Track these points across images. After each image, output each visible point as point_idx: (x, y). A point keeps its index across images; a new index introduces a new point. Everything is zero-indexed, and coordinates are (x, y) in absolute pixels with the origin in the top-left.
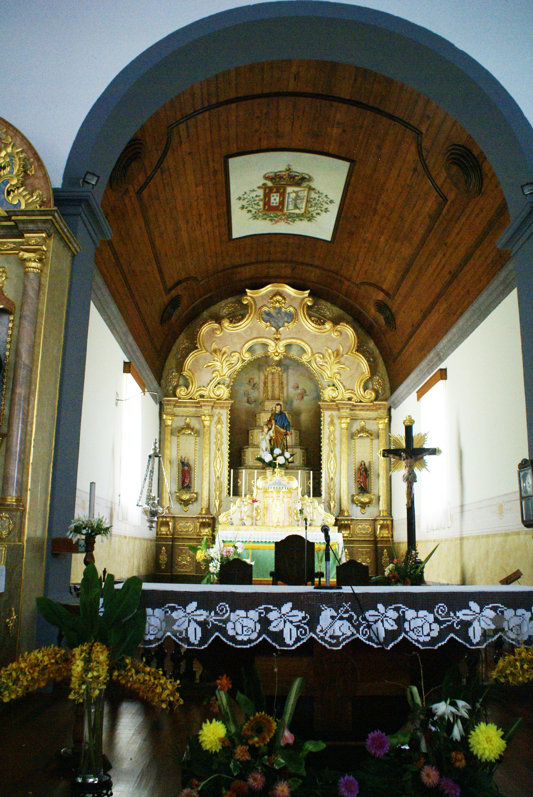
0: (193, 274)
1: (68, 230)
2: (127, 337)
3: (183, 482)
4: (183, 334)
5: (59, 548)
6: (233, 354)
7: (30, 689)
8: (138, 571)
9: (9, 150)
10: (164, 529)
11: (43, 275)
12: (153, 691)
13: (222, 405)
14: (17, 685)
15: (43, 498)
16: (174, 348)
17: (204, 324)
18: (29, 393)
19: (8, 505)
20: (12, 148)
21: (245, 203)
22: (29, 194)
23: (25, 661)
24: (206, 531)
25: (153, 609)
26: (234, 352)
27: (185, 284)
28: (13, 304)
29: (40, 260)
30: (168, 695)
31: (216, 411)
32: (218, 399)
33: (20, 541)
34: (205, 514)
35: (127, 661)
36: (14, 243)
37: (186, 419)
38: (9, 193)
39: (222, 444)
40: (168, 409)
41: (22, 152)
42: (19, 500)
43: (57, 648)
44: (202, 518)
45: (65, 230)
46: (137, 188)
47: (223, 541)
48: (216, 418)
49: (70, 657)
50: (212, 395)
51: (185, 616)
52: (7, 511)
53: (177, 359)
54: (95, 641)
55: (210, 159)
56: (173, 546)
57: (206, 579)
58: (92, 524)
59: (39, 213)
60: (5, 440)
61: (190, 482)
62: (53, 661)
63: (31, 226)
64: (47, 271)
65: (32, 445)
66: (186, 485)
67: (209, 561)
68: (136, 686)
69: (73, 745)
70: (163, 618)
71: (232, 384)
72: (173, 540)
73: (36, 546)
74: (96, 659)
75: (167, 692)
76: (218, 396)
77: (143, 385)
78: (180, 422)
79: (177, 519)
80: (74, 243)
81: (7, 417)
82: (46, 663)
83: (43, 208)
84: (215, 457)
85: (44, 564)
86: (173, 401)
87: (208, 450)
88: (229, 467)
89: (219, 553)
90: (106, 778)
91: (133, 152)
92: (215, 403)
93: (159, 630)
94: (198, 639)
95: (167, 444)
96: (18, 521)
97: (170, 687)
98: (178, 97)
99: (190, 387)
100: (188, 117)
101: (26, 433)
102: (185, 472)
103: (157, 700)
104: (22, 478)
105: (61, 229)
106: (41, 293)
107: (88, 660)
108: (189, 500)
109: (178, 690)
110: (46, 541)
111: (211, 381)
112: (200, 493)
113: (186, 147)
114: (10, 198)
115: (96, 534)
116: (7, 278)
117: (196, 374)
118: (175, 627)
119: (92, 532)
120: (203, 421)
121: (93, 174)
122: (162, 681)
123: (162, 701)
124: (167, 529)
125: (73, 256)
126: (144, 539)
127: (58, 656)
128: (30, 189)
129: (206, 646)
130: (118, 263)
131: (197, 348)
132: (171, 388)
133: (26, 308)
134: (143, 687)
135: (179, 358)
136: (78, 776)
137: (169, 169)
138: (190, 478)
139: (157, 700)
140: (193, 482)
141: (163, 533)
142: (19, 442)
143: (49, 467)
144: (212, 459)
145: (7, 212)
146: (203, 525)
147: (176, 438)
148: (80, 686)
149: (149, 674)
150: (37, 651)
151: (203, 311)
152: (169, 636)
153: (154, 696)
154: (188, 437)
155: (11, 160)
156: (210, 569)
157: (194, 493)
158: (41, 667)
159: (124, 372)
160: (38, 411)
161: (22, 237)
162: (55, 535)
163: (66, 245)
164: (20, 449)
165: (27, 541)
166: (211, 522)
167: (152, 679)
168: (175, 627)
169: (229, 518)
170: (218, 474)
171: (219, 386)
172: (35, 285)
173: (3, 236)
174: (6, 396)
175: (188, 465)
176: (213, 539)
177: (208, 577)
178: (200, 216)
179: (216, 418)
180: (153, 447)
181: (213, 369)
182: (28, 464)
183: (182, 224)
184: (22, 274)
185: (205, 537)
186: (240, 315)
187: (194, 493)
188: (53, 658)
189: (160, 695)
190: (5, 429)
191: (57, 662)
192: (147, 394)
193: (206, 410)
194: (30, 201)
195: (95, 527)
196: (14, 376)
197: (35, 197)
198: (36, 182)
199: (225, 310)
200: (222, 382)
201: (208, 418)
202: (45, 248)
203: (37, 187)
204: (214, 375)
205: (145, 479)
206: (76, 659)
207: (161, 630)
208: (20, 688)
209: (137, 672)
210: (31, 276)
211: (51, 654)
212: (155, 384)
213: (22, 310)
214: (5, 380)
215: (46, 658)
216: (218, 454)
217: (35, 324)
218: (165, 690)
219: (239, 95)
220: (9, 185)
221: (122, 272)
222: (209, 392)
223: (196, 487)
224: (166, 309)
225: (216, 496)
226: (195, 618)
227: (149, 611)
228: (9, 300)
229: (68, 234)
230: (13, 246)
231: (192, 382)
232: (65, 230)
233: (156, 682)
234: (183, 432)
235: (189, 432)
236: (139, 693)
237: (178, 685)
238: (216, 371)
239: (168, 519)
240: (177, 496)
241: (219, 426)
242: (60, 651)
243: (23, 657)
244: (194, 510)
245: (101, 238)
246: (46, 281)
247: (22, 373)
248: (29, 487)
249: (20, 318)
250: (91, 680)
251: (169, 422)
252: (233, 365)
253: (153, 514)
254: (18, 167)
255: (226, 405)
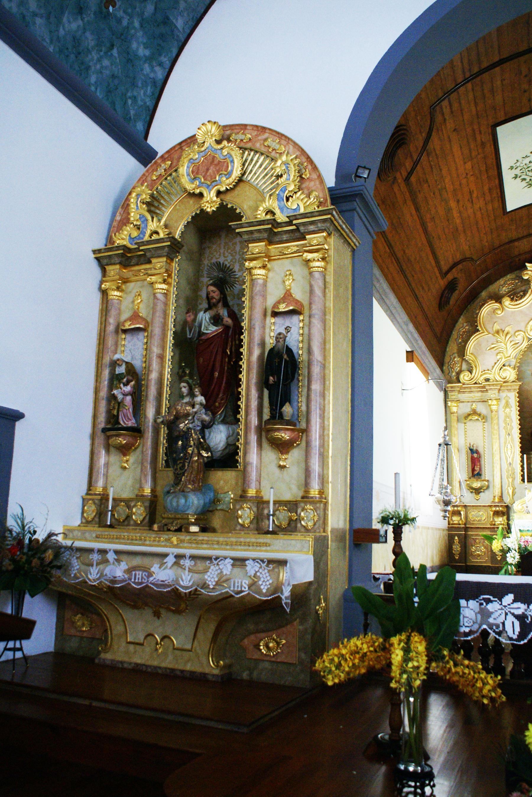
0: (468, 256)
1: (346, 226)
2: (407, 325)
3: (473, 470)
4: (462, 317)
5: (362, 537)
6: (517, 334)
7: (352, 675)
8: (433, 561)
9: (284, 158)
10: (456, 519)
11: (328, 273)
12: (473, 685)
13: (509, 388)
14: (339, 669)
15: (343, 490)
16: (455, 333)
17: (483, 305)
18: (324, 390)
19: (312, 498)
20: (287, 155)
21: (518, 172)
22: (306, 197)
23: (345, 647)
24: (500, 520)
25: (467, 600)
26: (518, 331)
27: (460, 266)
28: (302, 305)
29: (323, 259)
30: (489, 691)
31: (503, 394)
32: (505, 382)
33: (324, 532)
34: (499, 502)
35: (445, 653)
36: (297, 246)
37: (472, 405)
38: (288, 199)
39: (512, 428)
40: (452, 395)
41: (296, 158)
42: (321, 492)
43: (374, 637)
44: (495, 506)
45: (344, 226)
46: (405, 174)
47: (520, 530)
48: (503, 402)
49: (387, 646)
50: (498, 378)
51: (502, 609)
52: (311, 503)
53: (458, 345)
54: (412, 631)
55: (477, 133)
56: (466, 536)
57: (503, 571)
58: (399, 514)
59: (247, 225)
60: (305, 434)
61: (480, 469)
62: (372, 649)
63: (312, 228)
64: (331, 268)
65: (331, 439)
66: (476, 473)
67: (505, 551)
68: (456, 678)
69: (390, 732)
70: (477, 610)
71: (518, 365)
72: (466, 529)
73: (340, 536)
74: (415, 649)
75: (488, 687)
76: (504, 379)
77: (426, 372)
78: (466, 409)
79: (469, 508)
80: (353, 238)
81: (305, 413)
82: (365, 651)
83: (321, 209)
84: (505, 443)
85: (347, 553)
86: (458, 387)
87: (497, 436)
88: (521, 452)
89: (516, 543)
90: (427, 769)
91: (399, 138)
92: (501, 386)
93: (474, 623)
94: (517, 633)
95: (454, 431)
96: (322, 513)
97: (491, 682)
98: (438, 74)
99: (474, 371)
100: (449, 93)
101: (323, 428)
102: (475, 459)
103: (477, 694)
104: (323, 471)
105: (341, 226)
106: (327, 290)
107: (407, 650)
108: (480, 488)
109: (500, 686)
110: (348, 532)
111: (495, 363)
112: (491, 480)
113: (450, 125)
114: (289, 203)
115: (404, 524)
116: (293, 280)
117: (479, 358)
118: (491, 620)
119: (399, 522)
120: (490, 405)
121: (365, 168)
122: (483, 676)
123: (483, 696)
124: (459, 518)
125: (353, 251)
126: (436, 529)
127: (376, 644)
128: (306, 191)
129: (526, 641)
130: (393, 254)
131: (478, 330)
132: (454, 374)
133: (314, 307)
134: (462, 680)
135: (460, 343)
136: (399, 763)
137: (434, 149)
138: (480, 465)
139: (477, 694)
140: (483, 469)
141: (455, 522)
142: (318, 437)
143: (346, 459)
144: (502, 445)
145: (287, 217)
146: (497, 513)
147: (463, 425)
148: (401, 674)
149: (468, 667)
150: (355, 639)
151: (482, 292)
152: (485, 629)
153: (474, 691)
154: (475, 423)
155: (287, 167)
156: (508, 559)
157: (485, 480)
158: (361, 655)
159: (407, 361)
160: (333, 405)
161: (304, 239)
162: (356, 526)
163: (346, 241)
164: (319, 444)
165: (331, 532)
166: (505, 510)
167: (472, 673)
168: (491, 620)
169: (525, 505)
170: (510, 460)
171: (504, 368)
172: (321, 283)
173: (286, 240)
174: (303, 393)
175: (477, 452)
176: (508, 529)
177: (505, 568)
178: (471, 193)
179: (503, 402)
180: (443, 435)
181: (497, 351)
182: (328, 457)
183: (453, 204)
184: (308, 274)
185: (500, 527)
186: (522, 291)
187: (485, 480)
188: (372, 646)
189: (481, 690)
190: (303, 425)
191: (375, 651)
192: (431, 381)
193: (492, 394)
194: (308, 203)
195: (403, 517)
196: (309, 373)
197: (312, 199)
198: (312, 184)
199: (504, 289)
200: (507, 364)
201: (495, 402)
202: (326, 247)
203: (313, 188)
204: (498, 357)
205: (436, 468)
206: (395, 649)
207: (476, 622)
208: (342, 673)
209: (456, 665)
210: (317, 275)
211: (369, 642)
212: (438, 370)
213: (310, 308)
214: (300, 378)
215: (365, 646)
216: (509, 439)
217: (324, 322)
218: (486, 684)
219: (502, 58)
220: (287, 192)
221: (397, 260)
222: (495, 375)
223: (487, 474)
224: (442, 294)
225: (509, 484)
226: (512, 611)
227: (463, 602)
228: (297, 300)
229: (347, 230)
230: (295, 249)
231: (476, 367)
232: (344, 226)
233: (476, 676)
234: (470, 418)
235: (477, 418)
236: (458, 686)
237: (499, 680)
238: (499, 353)
239: (459, 509)
240: (468, 485)
241: (508, 410)
242: (377, 639)
243: (343, 643)
244: (486, 498)
245: (378, 230)
246: (330, 279)
247: (316, 370)
248: (330, 480)
249: (310, 317)
250: (411, 670)
251: (454, 409)
252: (518, 345)
253: (447, 503)
254: (293, 173)
255: (513, 388)
